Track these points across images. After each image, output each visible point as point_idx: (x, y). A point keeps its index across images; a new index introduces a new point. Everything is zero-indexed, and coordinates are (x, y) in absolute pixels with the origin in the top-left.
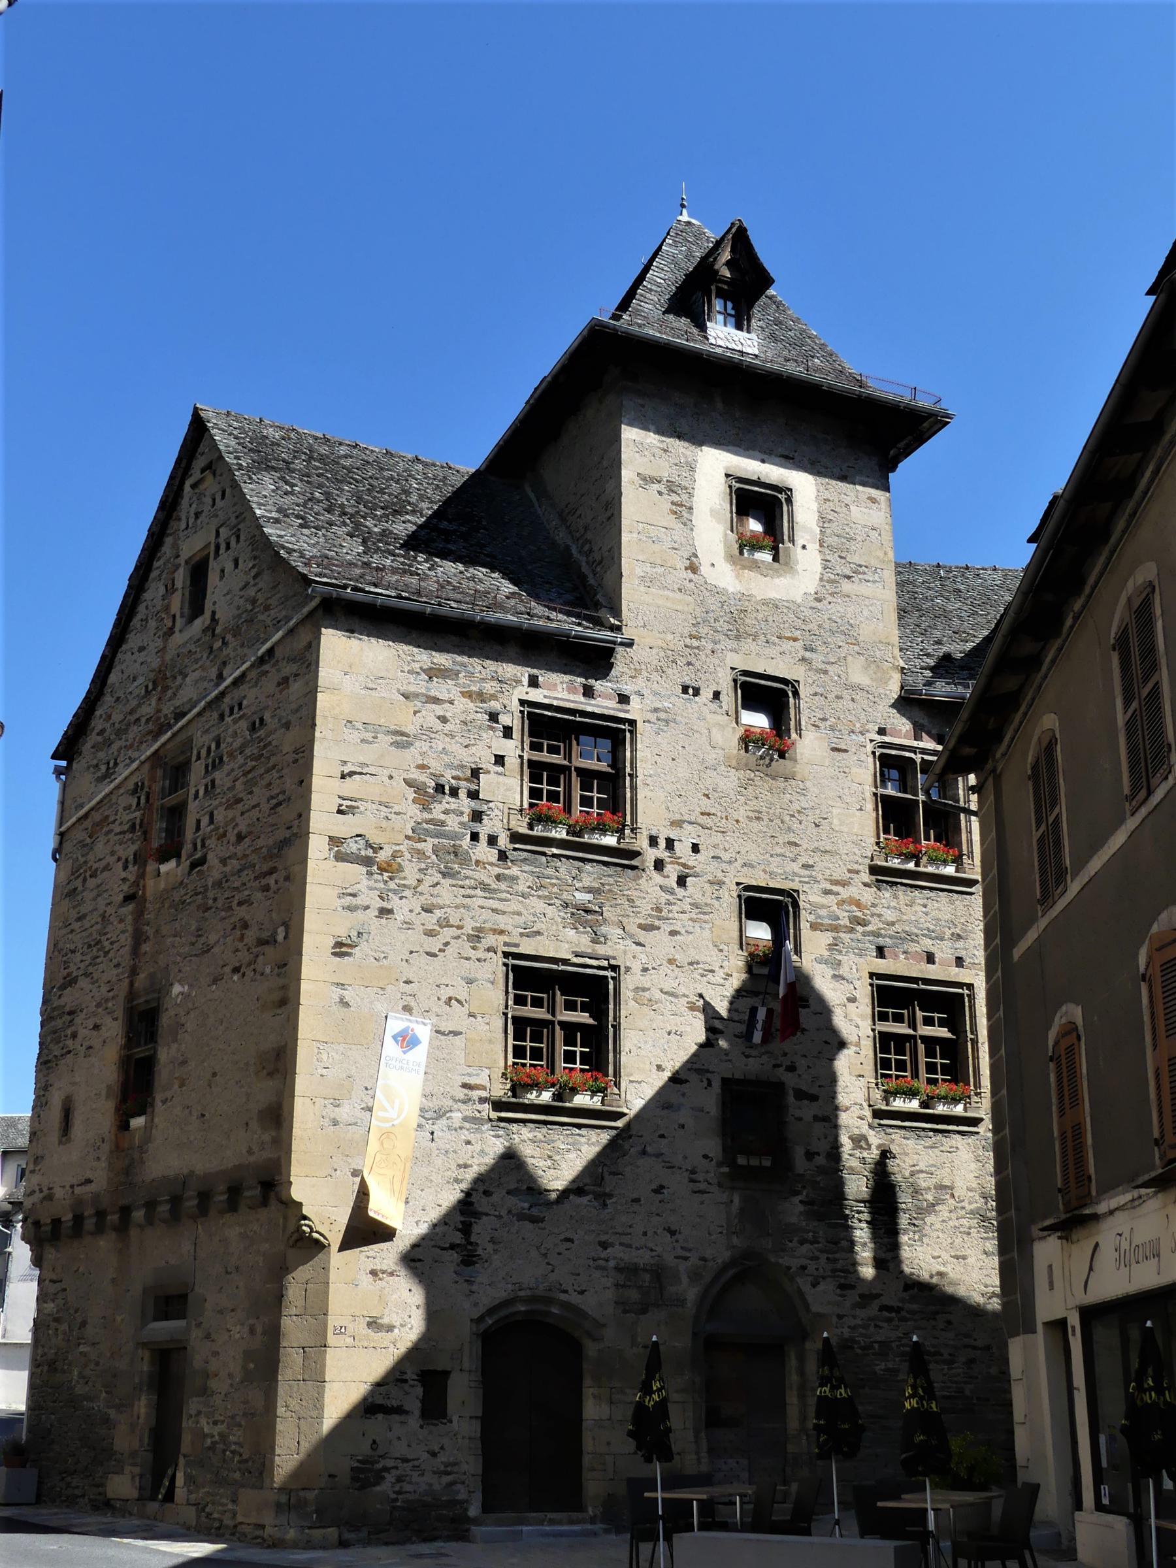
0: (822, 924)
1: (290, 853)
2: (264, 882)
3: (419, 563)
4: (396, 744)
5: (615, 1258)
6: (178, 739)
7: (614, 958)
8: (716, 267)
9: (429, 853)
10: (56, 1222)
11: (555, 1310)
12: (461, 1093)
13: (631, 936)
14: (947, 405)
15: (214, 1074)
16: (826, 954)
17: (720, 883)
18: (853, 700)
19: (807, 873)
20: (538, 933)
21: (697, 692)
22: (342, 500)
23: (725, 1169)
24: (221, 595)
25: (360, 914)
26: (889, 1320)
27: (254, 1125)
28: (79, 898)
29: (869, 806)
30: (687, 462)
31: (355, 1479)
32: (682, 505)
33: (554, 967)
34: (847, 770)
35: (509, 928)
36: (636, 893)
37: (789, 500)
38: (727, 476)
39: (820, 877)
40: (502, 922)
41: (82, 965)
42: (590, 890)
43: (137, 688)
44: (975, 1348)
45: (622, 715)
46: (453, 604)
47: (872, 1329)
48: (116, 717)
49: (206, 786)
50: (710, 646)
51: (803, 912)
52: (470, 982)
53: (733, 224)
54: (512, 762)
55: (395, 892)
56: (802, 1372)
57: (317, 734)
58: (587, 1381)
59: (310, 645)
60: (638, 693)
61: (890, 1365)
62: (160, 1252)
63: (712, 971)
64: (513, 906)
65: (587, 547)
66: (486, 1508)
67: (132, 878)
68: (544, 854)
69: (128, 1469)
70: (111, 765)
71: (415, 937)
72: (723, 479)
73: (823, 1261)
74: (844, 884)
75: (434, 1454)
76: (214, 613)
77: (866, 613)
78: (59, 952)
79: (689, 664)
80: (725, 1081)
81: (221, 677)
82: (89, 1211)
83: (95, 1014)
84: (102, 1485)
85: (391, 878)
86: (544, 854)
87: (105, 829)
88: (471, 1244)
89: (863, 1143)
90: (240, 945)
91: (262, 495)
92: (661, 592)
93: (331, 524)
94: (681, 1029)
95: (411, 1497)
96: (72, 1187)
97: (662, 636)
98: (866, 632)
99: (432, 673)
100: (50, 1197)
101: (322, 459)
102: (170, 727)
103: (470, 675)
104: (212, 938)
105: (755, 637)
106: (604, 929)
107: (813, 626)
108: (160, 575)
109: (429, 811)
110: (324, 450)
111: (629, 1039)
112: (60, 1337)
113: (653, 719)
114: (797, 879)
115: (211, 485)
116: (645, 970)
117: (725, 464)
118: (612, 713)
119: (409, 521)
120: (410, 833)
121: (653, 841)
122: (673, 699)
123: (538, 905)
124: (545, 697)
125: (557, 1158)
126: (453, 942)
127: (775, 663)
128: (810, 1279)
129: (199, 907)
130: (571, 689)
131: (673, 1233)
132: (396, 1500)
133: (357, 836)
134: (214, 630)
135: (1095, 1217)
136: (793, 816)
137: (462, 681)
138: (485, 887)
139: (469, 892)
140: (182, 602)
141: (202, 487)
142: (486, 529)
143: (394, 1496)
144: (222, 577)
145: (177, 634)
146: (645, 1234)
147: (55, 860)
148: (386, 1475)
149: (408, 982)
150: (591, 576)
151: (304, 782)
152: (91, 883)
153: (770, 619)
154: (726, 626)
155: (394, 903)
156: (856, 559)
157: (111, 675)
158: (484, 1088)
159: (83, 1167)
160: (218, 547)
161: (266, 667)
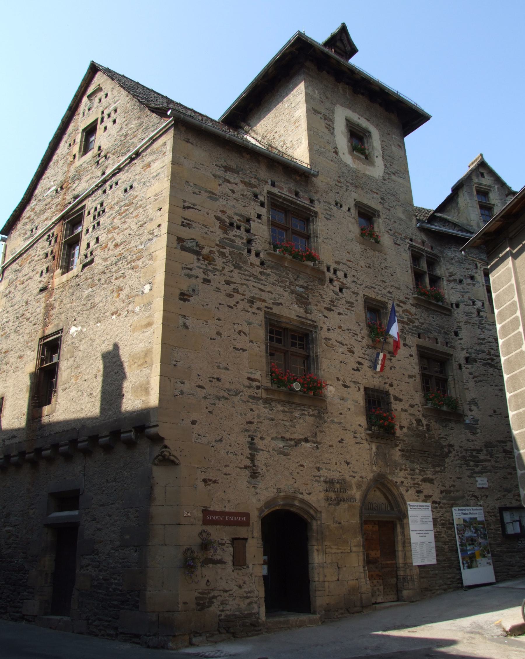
5: (323, 476)
7: (315, 322)
19: (390, 295)
25: (193, 281)
29: (410, 271)
31: (198, 604)
40: (264, 296)
45: (312, 208)
48: (37, 209)
54: (265, 218)
55: (210, 271)
63: (357, 335)
73: (410, 479)
75: (240, 587)
79: (338, 193)
81: (104, 173)
85: (210, 264)
95: (228, 613)
96: (4, 441)
99: (227, 169)
109: (228, 234)
116: (329, 330)
120: (218, 243)
124: (279, 192)
128: (405, 488)
130: (290, 190)
131: (348, 464)
132: (221, 615)
139: (247, 278)
143: (219, 613)
146: (336, 464)
148: (214, 600)
158: (258, 381)
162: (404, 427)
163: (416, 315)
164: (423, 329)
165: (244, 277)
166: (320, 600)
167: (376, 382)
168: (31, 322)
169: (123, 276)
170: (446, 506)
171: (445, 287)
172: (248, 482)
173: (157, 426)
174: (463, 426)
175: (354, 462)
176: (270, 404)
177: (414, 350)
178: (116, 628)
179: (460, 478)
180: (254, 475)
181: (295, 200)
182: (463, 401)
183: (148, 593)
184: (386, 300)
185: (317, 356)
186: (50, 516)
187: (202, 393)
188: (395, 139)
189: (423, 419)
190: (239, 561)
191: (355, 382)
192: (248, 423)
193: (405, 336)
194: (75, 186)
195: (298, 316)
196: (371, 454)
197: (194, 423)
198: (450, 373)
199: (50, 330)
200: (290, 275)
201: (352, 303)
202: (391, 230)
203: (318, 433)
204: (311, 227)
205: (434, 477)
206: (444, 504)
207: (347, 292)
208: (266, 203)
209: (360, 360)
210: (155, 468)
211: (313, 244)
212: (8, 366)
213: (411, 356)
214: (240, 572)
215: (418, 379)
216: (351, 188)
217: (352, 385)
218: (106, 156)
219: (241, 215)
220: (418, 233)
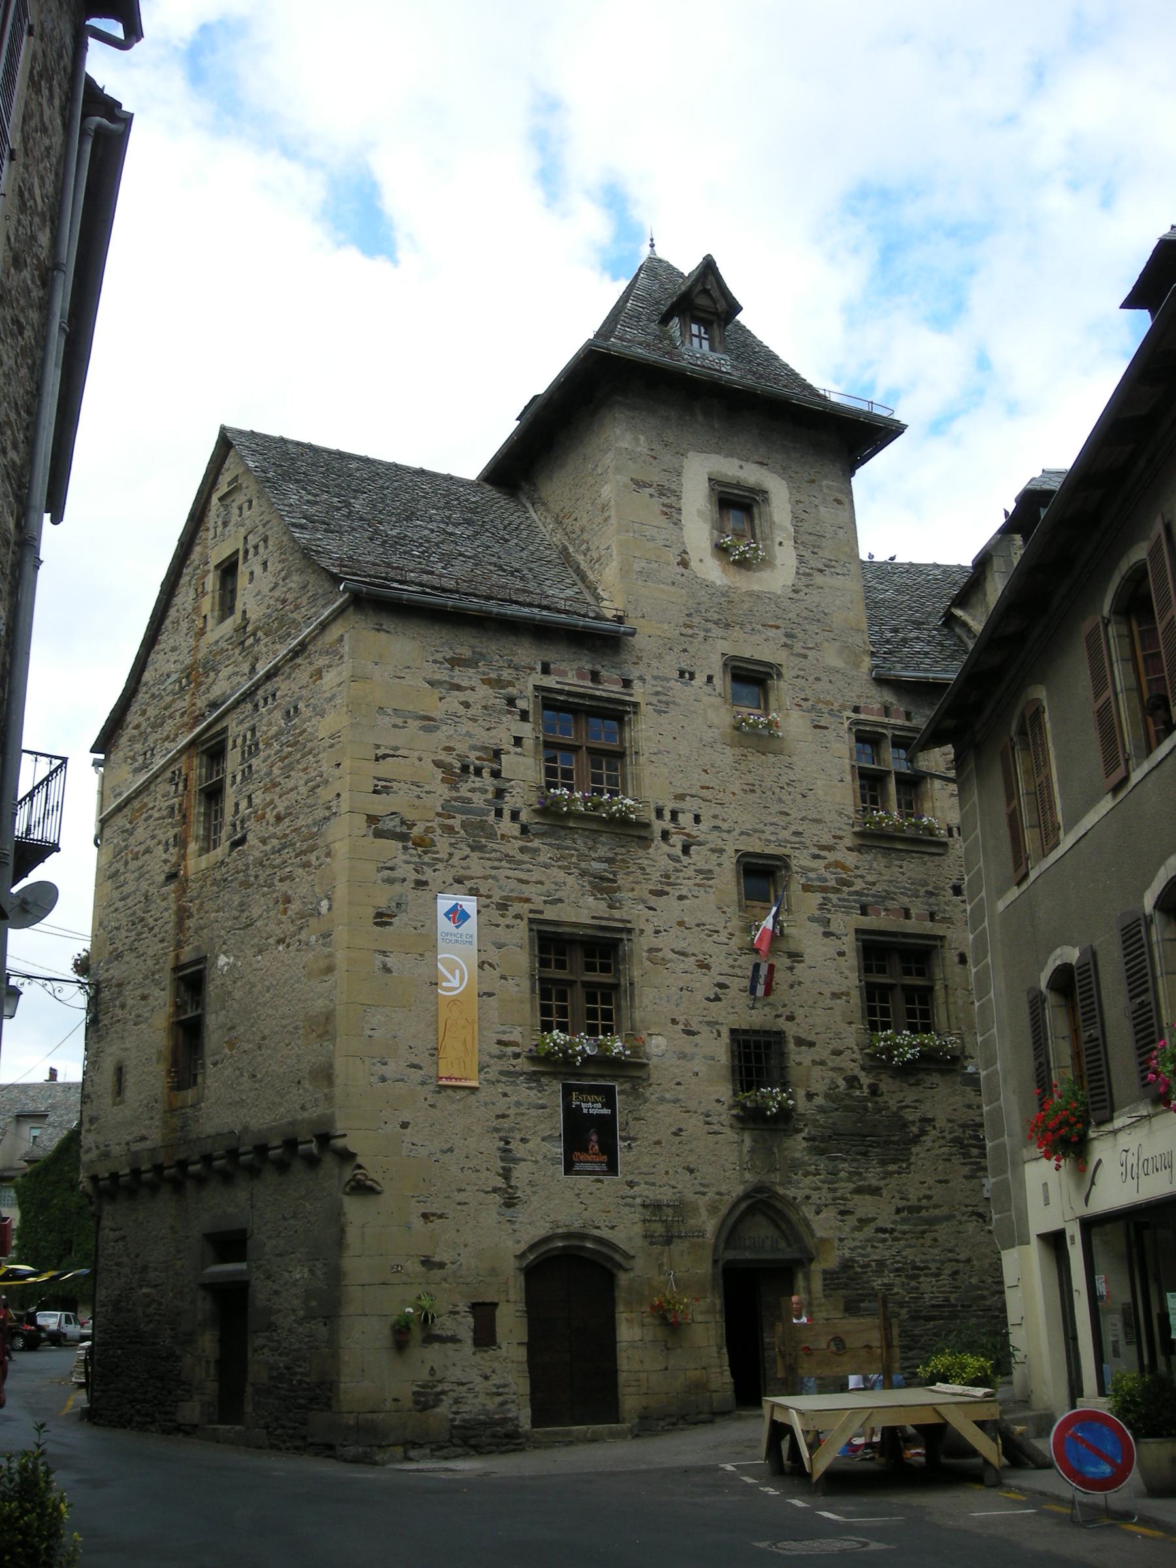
0: (813, 886)
5: (640, 1196)
7: (629, 922)
11: (589, 1245)
14: (900, 416)
15: (264, 1038)
16: (817, 913)
19: (798, 839)
20: (560, 900)
21: (692, 676)
25: (397, 887)
28: (122, 878)
29: (848, 778)
31: (416, 1402)
38: (710, 480)
39: (808, 843)
40: (528, 891)
44: (957, 1261)
45: (627, 698)
47: (869, 1249)
48: (152, 712)
49: (243, 771)
50: (702, 634)
52: (500, 946)
54: (528, 743)
55: (428, 865)
58: (620, 1308)
61: (886, 1281)
63: (717, 932)
65: (584, 547)
67: (173, 860)
73: (824, 1191)
75: (486, 1378)
76: (244, 612)
79: (685, 650)
80: (733, 1032)
81: (253, 670)
85: (426, 853)
87: (144, 815)
88: (511, 1187)
94: (692, 985)
95: (467, 1416)
96: (128, 1144)
99: (455, 662)
104: (256, 912)
105: (742, 625)
107: (792, 615)
108: (190, 581)
109: (457, 789)
116: (657, 932)
120: (440, 810)
121: (659, 813)
123: (561, 875)
124: (558, 683)
127: (761, 648)
128: (814, 1207)
130: (580, 675)
131: (691, 1171)
132: (453, 1420)
133: (393, 814)
134: (245, 627)
136: (782, 788)
139: (496, 864)
143: (451, 1416)
145: (209, 634)
146: (667, 1173)
148: (443, 1397)
152: (133, 865)
153: (755, 609)
158: (516, 1044)
161: (299, 661)
162: (817, 1095)
163: (857, 868)
164: (873, 896)
165: (489, 863)
166: (630, 1402)
167: (757, 1019)
168: (155, 936)
169: (290, 877)
170: (908, 1236)
171: (937, 794)
172: (499, 1214)
173: (344, 1135)
174: (959, 1079)
176: (538, 1081)
177: (849, 943)
178: (304, 1438)
179: (946, 1182)
180: (510, 1202)
181: (590, 692)
182: (964, 1028)
183: (342, 1385)
184: (787, 851)
185: (631, 984)
186: (209, 1270)
187: (417, 1075)
188: (828, 487)
189: (862, 1075)
190: (485, 1337)
191: (709, 1023)
192: (498, 1117)
193: (829, 916)
194: (210, 680)
195: (593, 918)
196: (741, 1152)
197: (405, 1125)
198: (938, 974)
199: (187, 954)
200: (579, 842)
201: (710, 871)
202: (806, 700)
203: (631, 1123)
204: (627, 736)
205: (882, 1183)
206: (904, 1233)
207: (698, 853)
208: (531, 711)
209: (722, 979)
210: (347, 1200)
211: (629, 769)
212: (126, 1011)
213: (841, 954)
214: (485, 1355)
215: (856, 999)
216: (716, 631)
217: (704, 1029)
218: (254, 634)
219: (484, 748)
220: (874, 691)
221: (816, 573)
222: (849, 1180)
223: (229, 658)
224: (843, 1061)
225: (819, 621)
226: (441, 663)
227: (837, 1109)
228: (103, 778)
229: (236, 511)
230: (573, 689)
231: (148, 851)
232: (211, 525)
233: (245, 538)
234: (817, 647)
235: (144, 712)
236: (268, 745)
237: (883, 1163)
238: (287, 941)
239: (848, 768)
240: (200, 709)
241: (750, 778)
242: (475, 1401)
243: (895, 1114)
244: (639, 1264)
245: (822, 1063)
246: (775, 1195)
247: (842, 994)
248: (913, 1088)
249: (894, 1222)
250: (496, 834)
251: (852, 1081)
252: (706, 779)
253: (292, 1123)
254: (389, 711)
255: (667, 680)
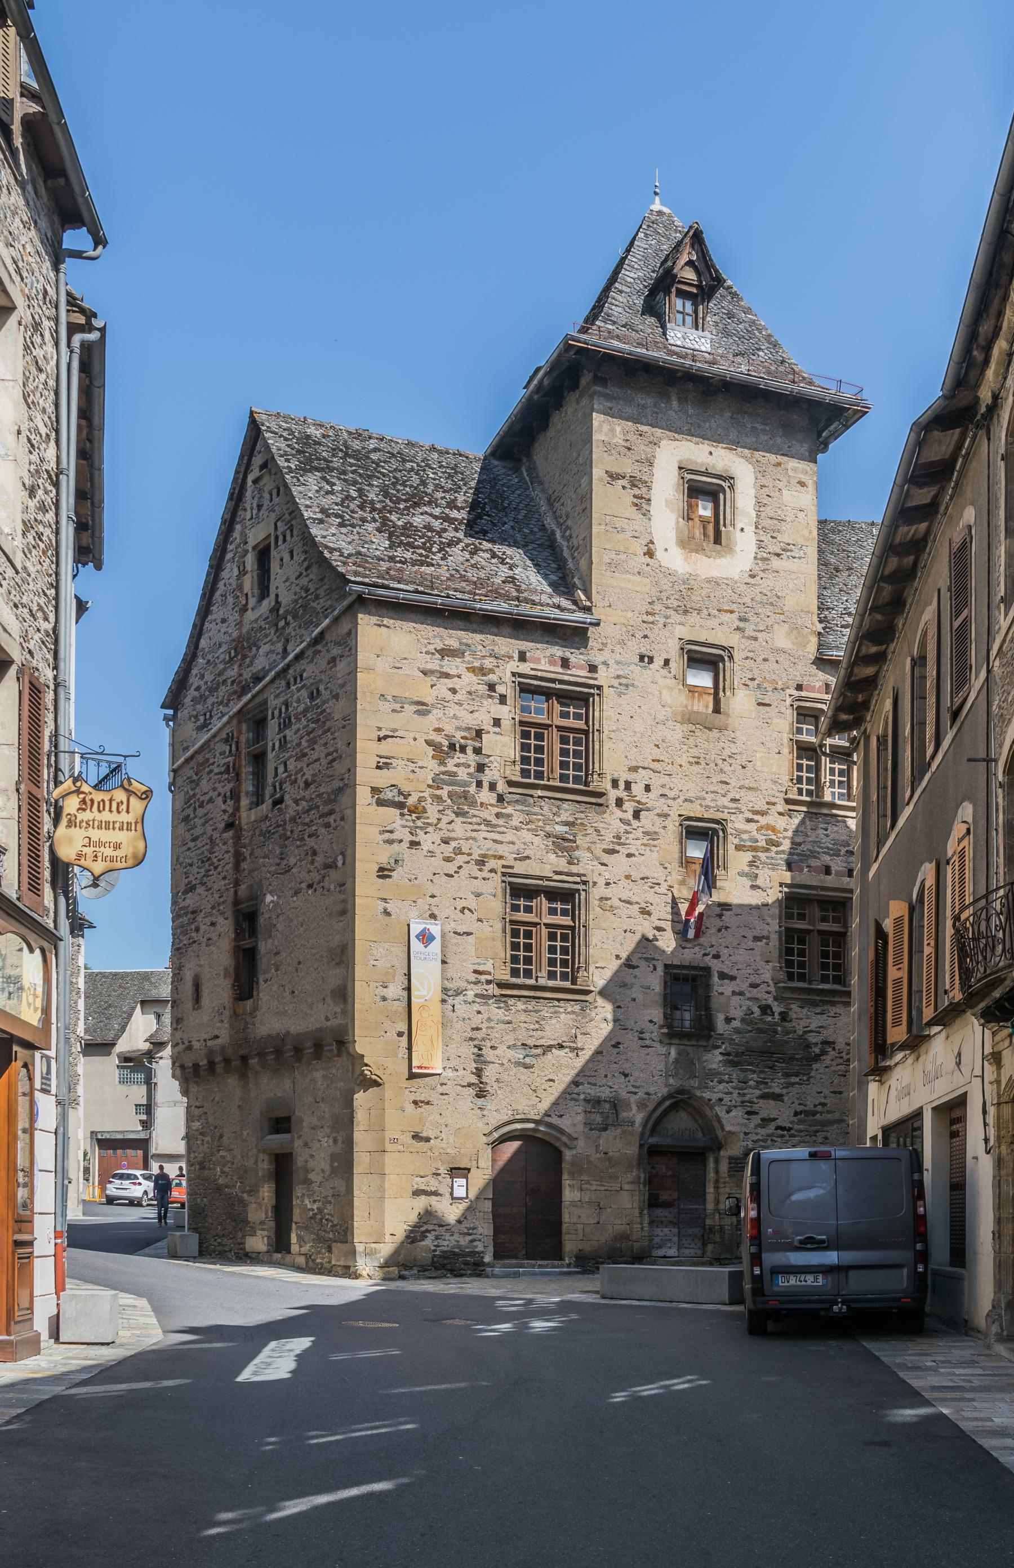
0: (744, 846)
1: (344, 799)
2: (326, 820)
3: (434, 554)
4: (418, 712)
6: (257, 701)
7: (584, 875)
8: (675, 271)
9: (445, 797)
10: (196, 1066)
12: (473, 977)
13: (598, 858)
15: (299, 963)
16: (747, 869)
17: (666, 816)
18: (777, 662)
20: (528, 858)
21: (651, 660)
22: (372, 496)
23: (665, 1030)
24: (284, 574)
26: (783, 1136)
27: (329, 1000)
28: (192, 823)
29: (786, 750)
30: (647, 459)
32: (642, 498)
33: (540, 882)
34: (769, 721)
35: (506, 854)
36: (602, 825)
37: (732, 487)
38: (680, 468)
39: (744, 809)
40: (501, 850)
41: (199, 876)
42: (566, 824)
43: (222, 654)
45: (592, 682)
46: (459, 595)
47: (769, 1142)
48: (209, 677)
50: (662, 620)
51: (730, 837)
52: (478, 895)
53: (691, 227)
54: (506, 724)
55: (421, 828)
56: (717, 1172)
57: (359, 707)
58: (565, 1176)
59: (349, 633)
60: (605, 663)
62: (269, 1088)
64: (509, 837)
66: (497, 1256)
67: (230, 811)
68: (532, 796)
69: (259, 1233)
70: (208, 717)
71: (437, 863)
72: (675, 472)
73: (735, 1095)
74: (763, 813)
76: (277, 596)
77: (791, 586)
78: (181, 864)
79: (646, 637)
82: (218, 1059)
83: (210, 914)
84: (243, 1244)
85: (418, 818)
86: (532, 796)
88: (481, 1083)
89: (769, 1011)
90: (312, 868)
91: (309, 493)
92: (623, 576)
93: (363, 520)
95: (445, 1249)
96: (205, 1040)
97: (624, 614)
98: (790, 603)
99: (445, 653)
100: (189, 1048)
101: (356, 455)
102: (250, 689)
103: (473, 654)
104: (292, 861)
105: (699, 611)
106: (577, 853)
107: (747, 600)
108: (233, 558)
110: (356, 445)
111: (596, 937)
112: (206, 1146)
113: (616, 685)
114: (726, 811)
115: (268, 483)
116: (608, 884)
117: (679, 458)
118: (583, 680)
119: (426, 513)
120: (430, 782)
121: (615, 783)
122: (633, 667)
123: (528, 836)
125: (542, 1023)
126: (464, 865)
127: (715, 632)
128: (725, 1108)
129: (280, 836)
131: (626, 1075)
132: (435, 1251)
134: (278, 610)
135: (889, 1068)
136: (724, 760)
137: (468, 658)
138: (487, 823)
139: (476, 827)
140: (252, 584)
141: (261, 483)
142: (489, 516)
143: (433, 1248)
144: (281, 566)
146: (606, 1076)
147: (172, 791)
149: (433, 896)
150: (570, 560)
151: (351, 743)
152: (200, 812)
154: (676, 603)
155: (421, 837)
156: (785, 538)
157: (202, 640)
158: (490, 974)
159: (211, 1025)
160: (277, 538)
161: (319, 647)
170: (802, 1134)
175: (636, 1074)
180: (481, 1094)
181: (560, 677)
184: (725, 816)
191: (647, 959)
193: (757, 872)
196: (667, 1062)
201: (655, 833)
202: (753, 679)
203: (579, 1036)
206: (800, 1131)
215: (774, 941)
216: (676, 618)
217: (643, 964)
221: (774, 558)
222: (756, 1088)
223: (266, 636)
224: (759, 993)
225: (772, 604)
226: (433, 654)
227: (751, 1031)
228: (174, 732)
229: (267, 496)
230: (544, 675)
231: (211, 800)
232: (248, 506)
233: (276, 524)
234: (768, 629)
235: (202, 677)
236: (298, 720)
237: (787, 1075)
238: (315, 886)
239: (786, 741)
240: (246, 680)
241: (694, 752)
242: (451, 1238)
243: (801, 1037)
244: (581, 1143)
245: (741, 994)
246: (692, 1096)
247: (763, 937)
248: (819, 1016)
249: (792, 1122)
250: (476, 802)
251: (766, 1009)
252: (657, 753)
253: (320, 1030)
254: (390, 698)
255: (629, 665)
